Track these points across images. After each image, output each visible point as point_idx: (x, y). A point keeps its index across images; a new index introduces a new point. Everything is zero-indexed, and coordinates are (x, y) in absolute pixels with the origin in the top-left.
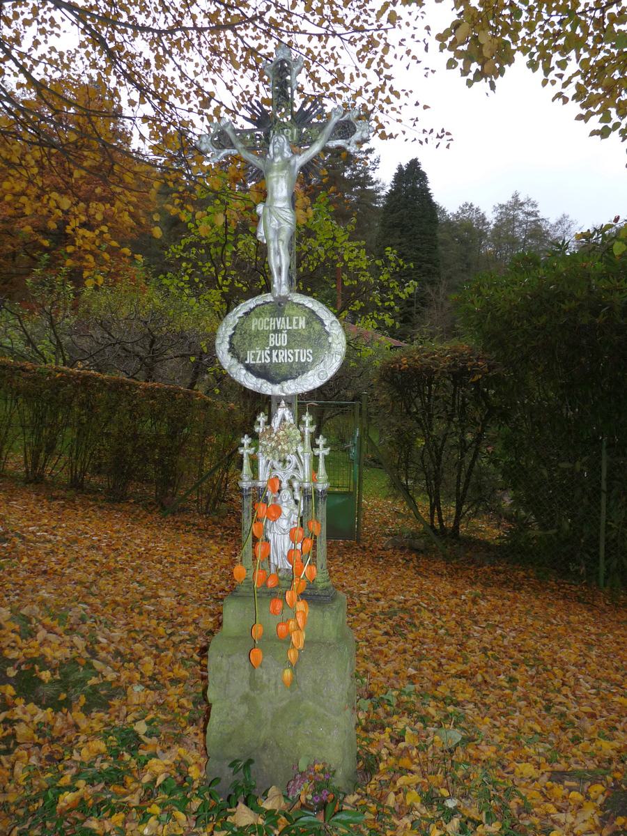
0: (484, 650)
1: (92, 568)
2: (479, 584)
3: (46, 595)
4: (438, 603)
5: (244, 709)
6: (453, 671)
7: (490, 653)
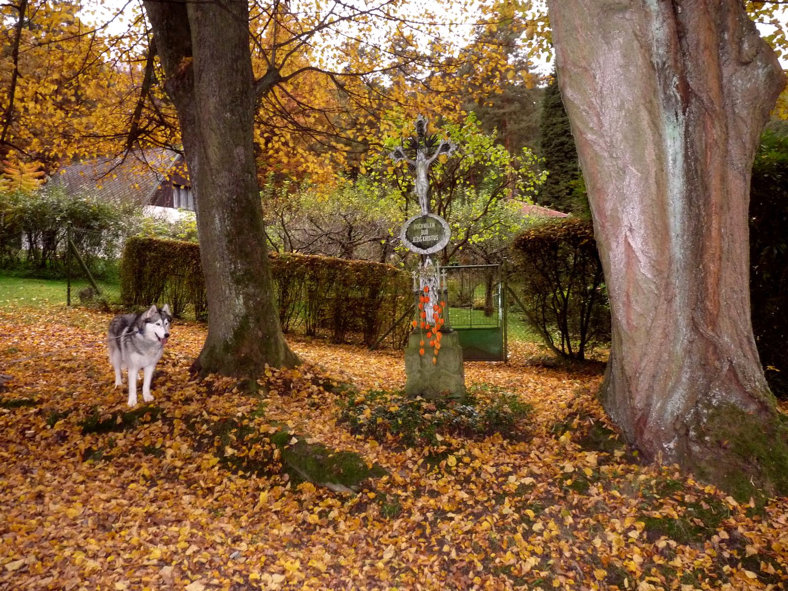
5: (419, 375)
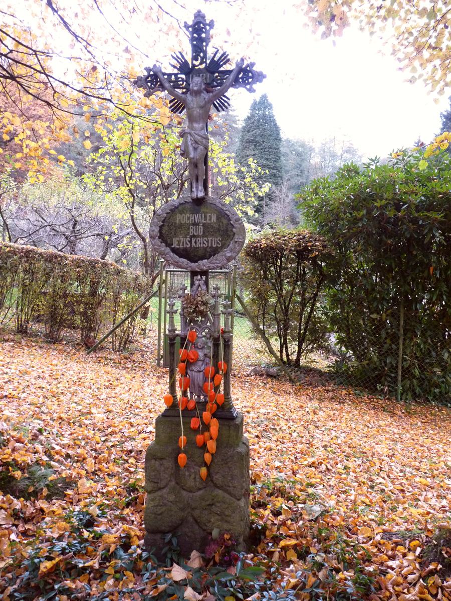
0: (325, 447)
1: (39, 392)
2: (315, 400)
3: (10, 414)
4: (291, 414)
6: (306, 463)
7: (329, 449)
